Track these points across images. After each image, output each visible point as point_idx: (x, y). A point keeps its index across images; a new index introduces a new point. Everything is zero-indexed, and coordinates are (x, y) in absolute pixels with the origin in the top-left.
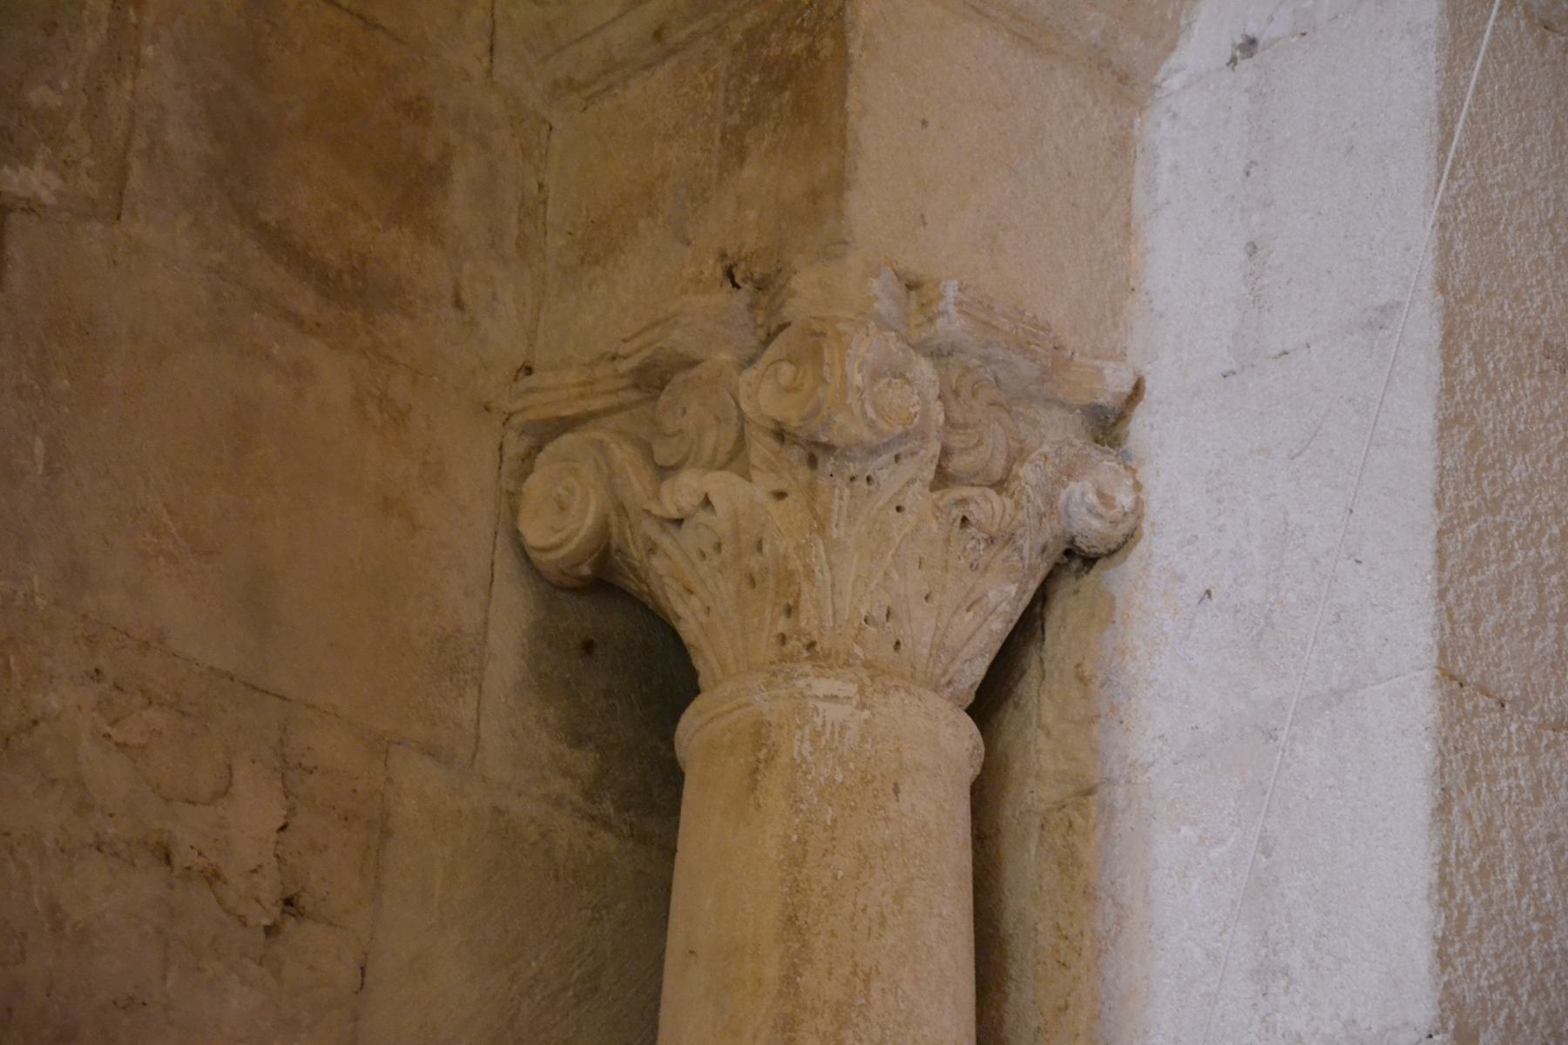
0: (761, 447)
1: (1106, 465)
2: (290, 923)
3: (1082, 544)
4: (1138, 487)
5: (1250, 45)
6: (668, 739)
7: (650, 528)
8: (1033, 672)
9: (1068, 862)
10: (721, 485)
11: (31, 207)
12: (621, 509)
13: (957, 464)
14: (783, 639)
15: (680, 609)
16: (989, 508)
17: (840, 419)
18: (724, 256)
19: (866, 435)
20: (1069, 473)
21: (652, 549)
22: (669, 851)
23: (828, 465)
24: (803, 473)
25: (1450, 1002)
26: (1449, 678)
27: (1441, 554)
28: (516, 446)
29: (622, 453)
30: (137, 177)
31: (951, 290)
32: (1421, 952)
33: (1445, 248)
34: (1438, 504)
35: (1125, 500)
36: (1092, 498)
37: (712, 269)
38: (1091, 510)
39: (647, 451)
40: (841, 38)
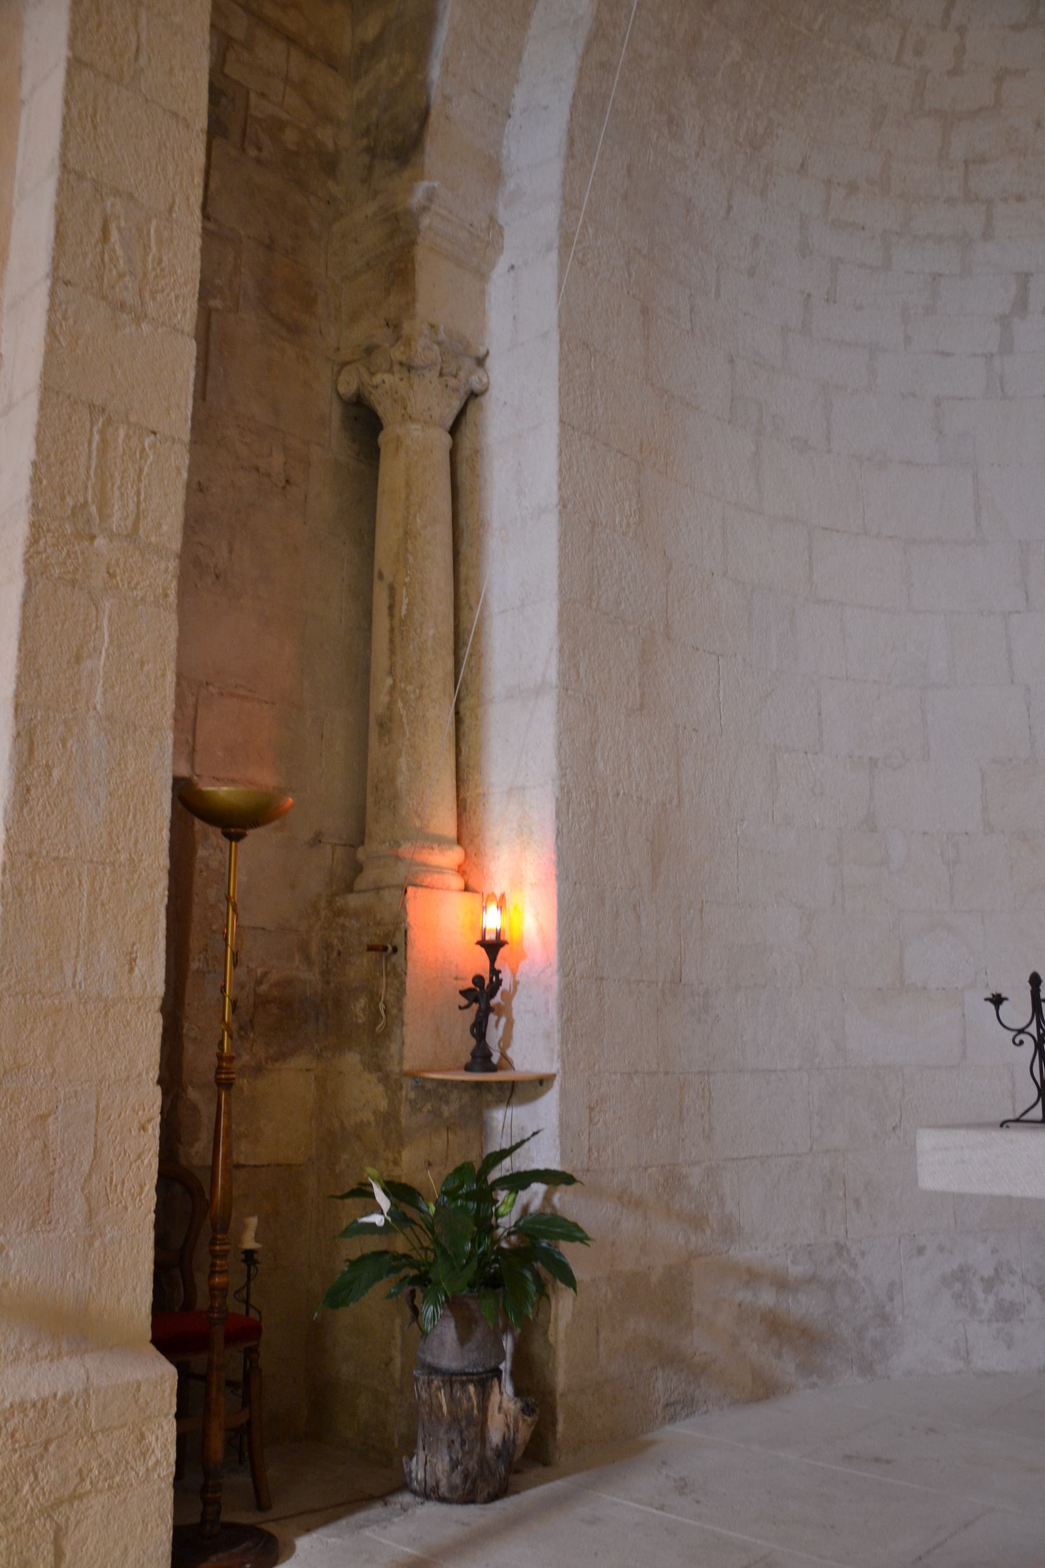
0: (396, 368)
1: (480, 372)
2: (288, 487)
3: (475, 391)
4: (488, 377)
5: (513, 267)
6: (376, 442)
7: (370, 388)
8: (464, 424)
9: (473, 469)
10: (387, 377)
11: (217, 310)
12: (363, 384)
13: (445, 371)
14: (403, 415)
15: (378, 408)
16: (452, 382)
17: (416, 360)
18: (385, 319)
19: (422, 364)
20: (471, 373)
21: (370, 393)
22: (377, 468)
23: (413, 372)
24: (407, 374)
25: (561, 498)
26: (562, 422)
27: (560, 393)
28: (336, 368)
29: (363, 370)
30: (241, 302)
31: (442, 328)
32: (555, 487)
33: (560, 317)
34: (559, 379)
35: (485, 380)
36: (477, 380)
37: (383, 322)
38: (477, 383)
39: (368, 369)
40: (413, 263)
